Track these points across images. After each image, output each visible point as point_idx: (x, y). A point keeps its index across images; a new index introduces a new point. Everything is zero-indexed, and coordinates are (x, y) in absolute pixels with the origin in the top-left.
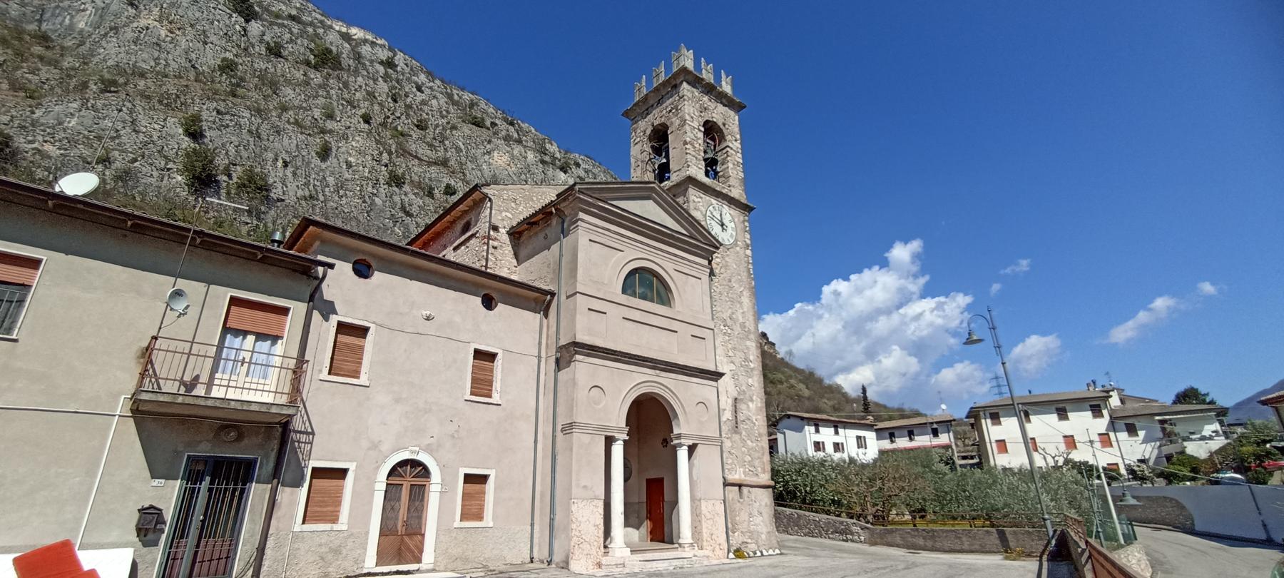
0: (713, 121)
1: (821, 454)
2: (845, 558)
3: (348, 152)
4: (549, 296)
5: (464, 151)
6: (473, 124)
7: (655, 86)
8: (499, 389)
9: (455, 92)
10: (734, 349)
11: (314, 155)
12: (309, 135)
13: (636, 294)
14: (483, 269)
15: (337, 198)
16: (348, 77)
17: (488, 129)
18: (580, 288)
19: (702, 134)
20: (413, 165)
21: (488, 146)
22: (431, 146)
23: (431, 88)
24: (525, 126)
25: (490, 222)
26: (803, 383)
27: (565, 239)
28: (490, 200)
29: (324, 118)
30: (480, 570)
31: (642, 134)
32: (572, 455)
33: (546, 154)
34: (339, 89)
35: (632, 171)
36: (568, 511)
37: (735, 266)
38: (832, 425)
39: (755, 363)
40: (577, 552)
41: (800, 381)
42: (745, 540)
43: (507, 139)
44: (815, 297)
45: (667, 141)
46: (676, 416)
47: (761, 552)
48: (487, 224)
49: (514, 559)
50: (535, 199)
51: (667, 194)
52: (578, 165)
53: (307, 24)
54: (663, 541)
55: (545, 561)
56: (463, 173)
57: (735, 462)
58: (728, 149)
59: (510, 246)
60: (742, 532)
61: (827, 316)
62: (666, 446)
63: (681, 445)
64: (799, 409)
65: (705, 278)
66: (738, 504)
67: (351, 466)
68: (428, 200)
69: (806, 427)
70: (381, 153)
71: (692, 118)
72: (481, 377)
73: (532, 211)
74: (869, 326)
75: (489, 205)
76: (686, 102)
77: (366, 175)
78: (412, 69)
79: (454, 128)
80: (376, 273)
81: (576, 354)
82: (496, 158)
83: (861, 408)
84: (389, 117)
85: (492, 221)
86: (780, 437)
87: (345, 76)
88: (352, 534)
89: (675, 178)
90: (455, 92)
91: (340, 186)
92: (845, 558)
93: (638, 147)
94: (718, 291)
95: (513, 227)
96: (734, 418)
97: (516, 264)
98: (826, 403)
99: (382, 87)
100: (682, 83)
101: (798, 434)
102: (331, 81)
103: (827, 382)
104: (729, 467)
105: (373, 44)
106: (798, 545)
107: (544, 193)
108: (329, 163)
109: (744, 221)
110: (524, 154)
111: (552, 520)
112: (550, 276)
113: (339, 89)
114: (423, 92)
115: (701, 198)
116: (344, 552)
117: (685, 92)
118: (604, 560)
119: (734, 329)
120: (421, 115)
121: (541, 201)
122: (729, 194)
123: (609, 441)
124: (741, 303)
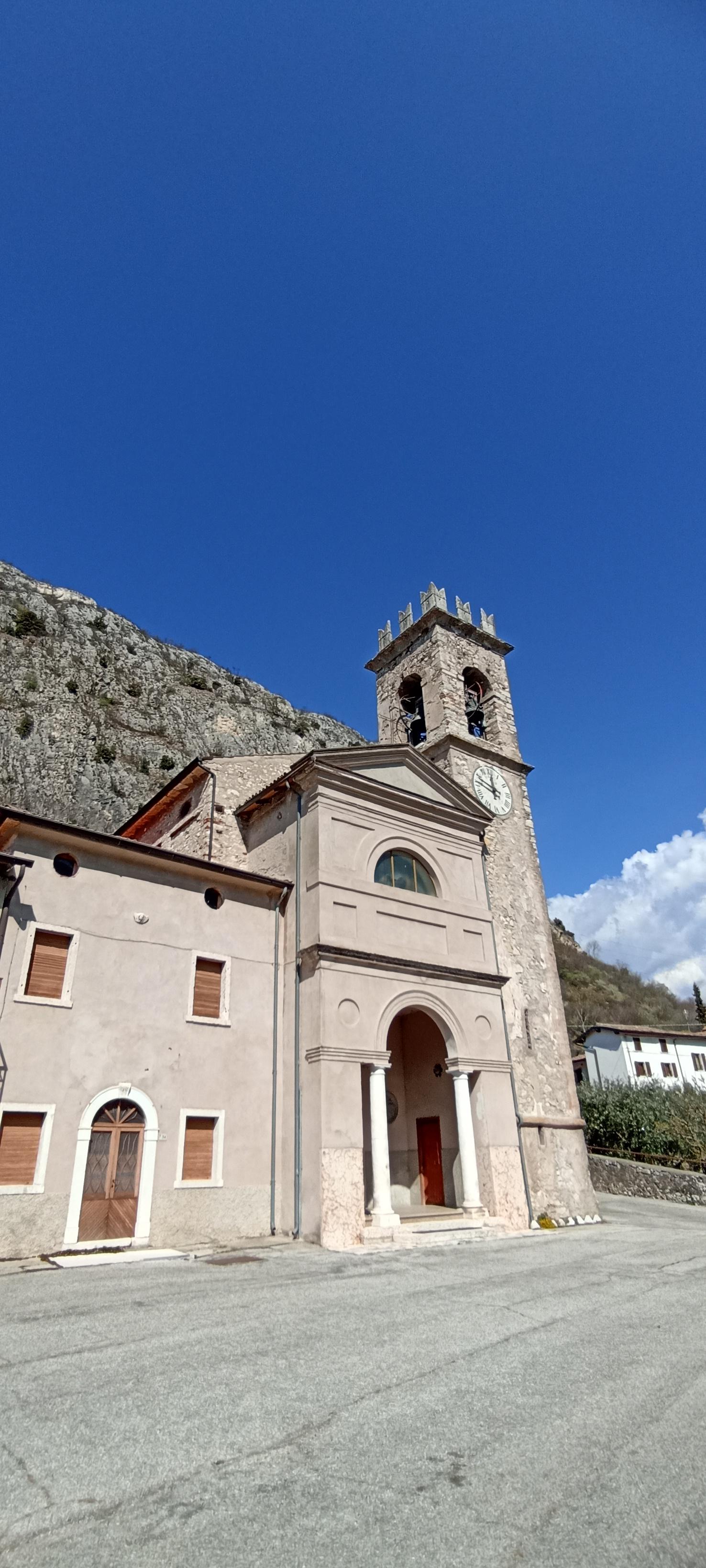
0: (474, 668)
1: (644, 1079)
2: (692, 1229)
3: (51, 727)
4: (285, 889)
5: (183, 717)
6: (193, 686)
7: (402, 631)
8: (227, 1006)
9: (171, 651)
10: (520, 945)
11: (13, 730)
12: (9, 709)
13: (391, 881)
14: (206, 859)
15: (38, 779)
16: (53, 643)
17: (210, 690)
18: (322, 878)
19: (462, 684)
20: (124, 737)
21: (210, 710)
22: (145, 714)
23: (144, 648)
24: (253, 684)
25: (213, 801)
26: (615, 983)
27: (303, 819)
28: (213, 776)
29: (25, 689)
30: (207, 1246)
31: (390, 688)
32: (320, 1089)
33: (278, 716)
34: (43, 656)
35: (380, 731)
36: (317, 1164)
37: (513, 841)
38: (657, 1039)
39: (548, 962)
40: (331, 1220)
41: (610, 981)
42: (552, 1203)
43: (233, 700)
44: (616, 871)
45: (421, 694)
46: (450, 1035)
47: (575, 1220)
48: (210, 805)
49: (251, 1231)
50: (265, 771)
51: (423, 758)
52: (316, 726)
53: (10, 590)
54: (442, 1203)
55: (290, 1234)
56: (182, 743)
57: (532, 1094)
58: (495, 699)
59: (238, 829)
60: (547, 1191)
61: (630, 894)
62: (440, 1075)
63: (458, 1073)
64: (612, 1019)
65: (477, 857)
66: (539, 1152)
67: (50, 1110)
68: (142, 776)
69: (624, 1044)
70: (88, 725)
71: (449, 665)
72: (205, 991)
73: (262, 787)
74: (690, 905)
75: (211, 782)
76: (440, 648)
77: (72, 750)
78: (123, 629)
79: (171, 691)
80: (81, 869)
81: (320, 959)
82: (220, 724)
83: (695, 1015)
84: (97, 684)
85: (216, 800)
86: (589, 1057)
87: (49, 642)
88: (49, 1199)
89: (432, 738)
90: (171, 651)
91: (42, 765)
92: (692, 1229)
93: (386, 704)
94: (494, 873)
95: (240, 807)
96: (526, 1035)
97: (245, 851)
98: (646, 1010)
99: (91, 651)
100: (434, 626)
101: (613, 1052)
102: (34, 648)
103: (645, 982)
104: (524, 1101)
105: (80, 605)
106: (625, 1210)
107: (276, 764)
108: (29, 740)
109: (521, 784)
110: (252, 716)
111: (297, 1176)
112: (287, 864)
113: (43, 656)
114: (135, 654)
115: (466, 760)
116: (39, 1222)
117: (439, 637)
118: (367, 1232)
119: (518, 920)
120: (133, 679)
121: (273, 774)
122: (500, 753)
123: (367, 1070)
124: (524, 887)
